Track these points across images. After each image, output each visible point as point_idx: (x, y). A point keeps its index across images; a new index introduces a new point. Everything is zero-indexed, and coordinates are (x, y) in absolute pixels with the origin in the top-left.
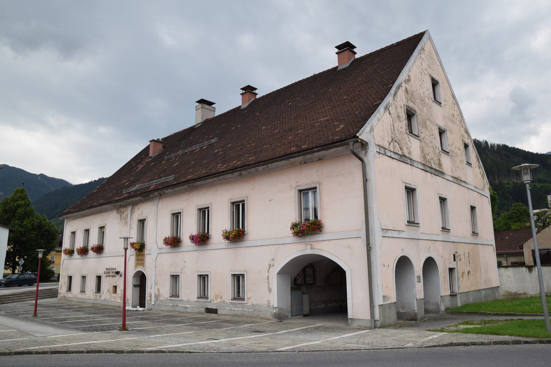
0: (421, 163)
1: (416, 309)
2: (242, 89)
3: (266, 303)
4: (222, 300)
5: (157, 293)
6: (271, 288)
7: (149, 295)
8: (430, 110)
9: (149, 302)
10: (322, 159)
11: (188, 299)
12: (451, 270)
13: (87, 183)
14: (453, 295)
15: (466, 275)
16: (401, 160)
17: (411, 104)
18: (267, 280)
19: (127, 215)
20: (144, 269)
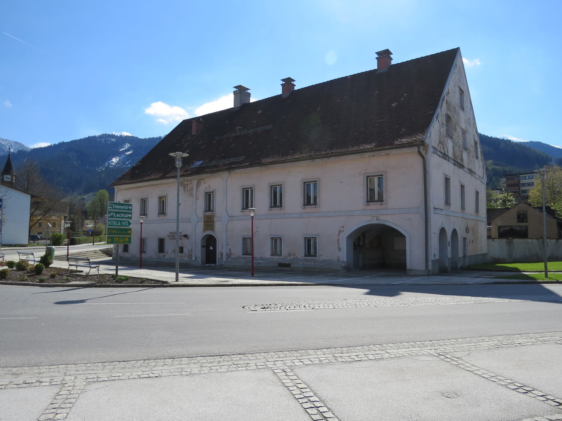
0: (453, 159)
1: (447, 265)
2: (283, 80)
3: (336, 259)
4: (295, 257)
5: (228, 252)
6: (341, 248)
7: (220, 254)
8: (458, 116)
9: (220, 259)
10: (388, 154)
11: (261, 256)
12: (465, 238)
13: (46, 147)
14: (465, 256)
15: (471, 243)
16: (444, 157)
17: (449, 113)
18: (337, 242)
19: (192, 188)
20: (214, 233)
